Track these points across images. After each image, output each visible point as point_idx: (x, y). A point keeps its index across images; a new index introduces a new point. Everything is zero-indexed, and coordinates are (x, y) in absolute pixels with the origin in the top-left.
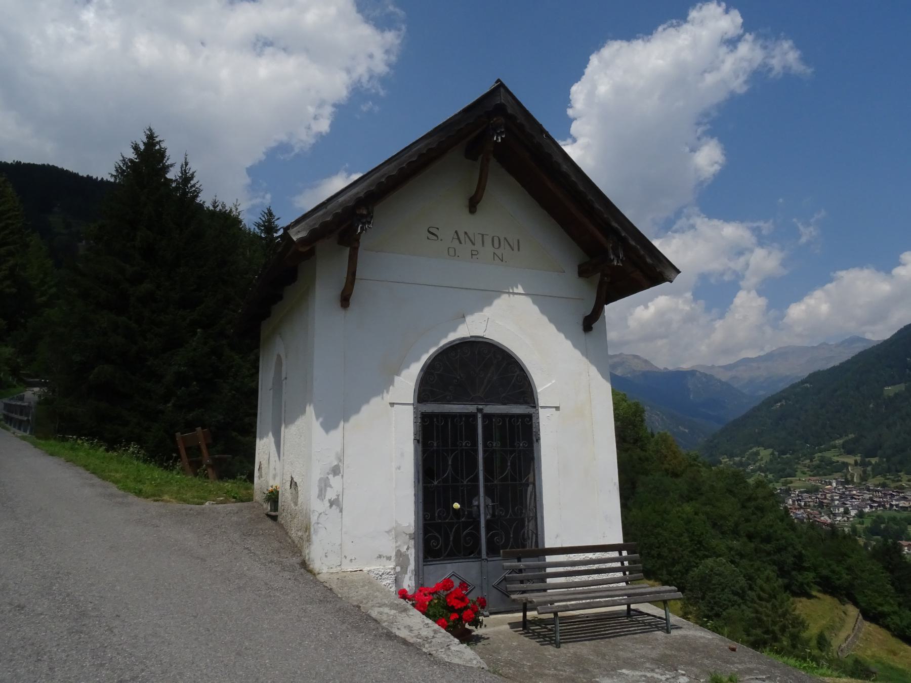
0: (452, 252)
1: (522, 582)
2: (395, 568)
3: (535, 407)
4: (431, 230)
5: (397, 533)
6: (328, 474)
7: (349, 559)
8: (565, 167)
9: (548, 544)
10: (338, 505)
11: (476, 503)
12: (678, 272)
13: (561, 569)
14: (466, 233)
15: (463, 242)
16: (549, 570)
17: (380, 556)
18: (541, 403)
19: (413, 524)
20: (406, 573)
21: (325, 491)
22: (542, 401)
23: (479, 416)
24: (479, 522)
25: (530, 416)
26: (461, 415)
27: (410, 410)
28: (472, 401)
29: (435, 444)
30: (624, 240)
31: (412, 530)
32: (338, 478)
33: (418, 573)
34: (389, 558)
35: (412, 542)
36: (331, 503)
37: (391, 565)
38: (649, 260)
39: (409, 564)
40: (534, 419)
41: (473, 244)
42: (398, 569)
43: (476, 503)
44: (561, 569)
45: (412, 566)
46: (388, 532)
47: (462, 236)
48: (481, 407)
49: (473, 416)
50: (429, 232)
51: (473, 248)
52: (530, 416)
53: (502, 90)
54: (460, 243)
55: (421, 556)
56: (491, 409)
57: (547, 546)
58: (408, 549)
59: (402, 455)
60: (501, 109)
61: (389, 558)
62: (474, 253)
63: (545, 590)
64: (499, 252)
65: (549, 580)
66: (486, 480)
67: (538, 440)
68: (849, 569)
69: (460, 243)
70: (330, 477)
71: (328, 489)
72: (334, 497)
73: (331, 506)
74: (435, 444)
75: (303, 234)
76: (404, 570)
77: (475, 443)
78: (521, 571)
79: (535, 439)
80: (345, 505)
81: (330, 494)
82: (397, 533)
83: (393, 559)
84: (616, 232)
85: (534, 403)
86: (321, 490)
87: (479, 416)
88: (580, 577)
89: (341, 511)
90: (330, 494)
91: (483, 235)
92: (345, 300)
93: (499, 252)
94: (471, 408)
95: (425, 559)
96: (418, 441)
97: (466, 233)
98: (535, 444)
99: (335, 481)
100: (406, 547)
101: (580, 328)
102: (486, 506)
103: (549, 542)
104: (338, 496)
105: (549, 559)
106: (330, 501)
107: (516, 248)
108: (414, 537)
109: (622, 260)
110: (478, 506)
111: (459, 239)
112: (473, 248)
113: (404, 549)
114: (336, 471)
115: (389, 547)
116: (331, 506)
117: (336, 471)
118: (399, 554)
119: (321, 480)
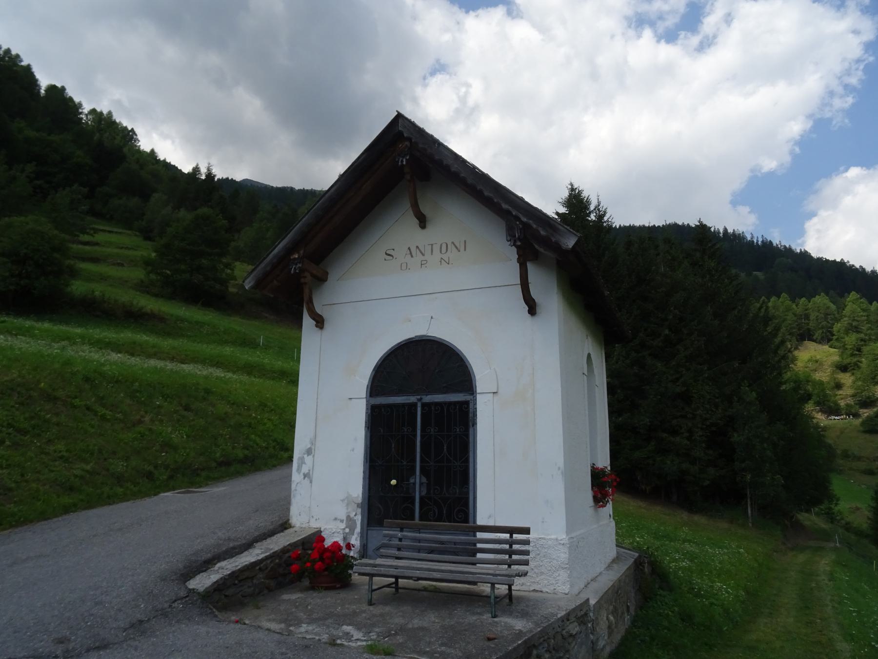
0: (404, 266)
5: (348, 501)
8: (455, 168)
10: (309, 478)
15: (414, 254)
17: (336, 519)
18: (478, 390)
19: (361, 496)
22: (481, 384)
23: (419, 405)
26: (403, 405)
27: (364, 402)
31: (360, 500)
32: (311, 457)
34: (342, 521)
35: (359, 510)
36: (305, 476)
37: (343, 526)
38: (543, 233)
40: (471, 406)
41: (423, 255)
42: (347, 530)
45: (358, 529)
46: (343, 501)
47: (413, 249)
49: (414, 406)
52: (467, 403)
53: (400, 121)
56: (428, 399)
60: (400, 136)
61: (342, 521)
64: (445, 257)
67: (474, 424)
70: (305, 456)
79: (471, 424)
81: (305, 469)
87: (419, 405)
89: (311, 482)
90: (305, 469)
92: (320, 322)
93: (445, 257)
94: (412, 399)
95: (369, 525)
97: (417, 247)
99: (308, 459)
102: (421, 484)
103: (481, 521)
107: (462, 249)
108: (360, 505)
109: (519, 239)
110: (414, 484)
111: (411, 253)
112: (423, 258)
114: (309, 452)
118: (349, 518)
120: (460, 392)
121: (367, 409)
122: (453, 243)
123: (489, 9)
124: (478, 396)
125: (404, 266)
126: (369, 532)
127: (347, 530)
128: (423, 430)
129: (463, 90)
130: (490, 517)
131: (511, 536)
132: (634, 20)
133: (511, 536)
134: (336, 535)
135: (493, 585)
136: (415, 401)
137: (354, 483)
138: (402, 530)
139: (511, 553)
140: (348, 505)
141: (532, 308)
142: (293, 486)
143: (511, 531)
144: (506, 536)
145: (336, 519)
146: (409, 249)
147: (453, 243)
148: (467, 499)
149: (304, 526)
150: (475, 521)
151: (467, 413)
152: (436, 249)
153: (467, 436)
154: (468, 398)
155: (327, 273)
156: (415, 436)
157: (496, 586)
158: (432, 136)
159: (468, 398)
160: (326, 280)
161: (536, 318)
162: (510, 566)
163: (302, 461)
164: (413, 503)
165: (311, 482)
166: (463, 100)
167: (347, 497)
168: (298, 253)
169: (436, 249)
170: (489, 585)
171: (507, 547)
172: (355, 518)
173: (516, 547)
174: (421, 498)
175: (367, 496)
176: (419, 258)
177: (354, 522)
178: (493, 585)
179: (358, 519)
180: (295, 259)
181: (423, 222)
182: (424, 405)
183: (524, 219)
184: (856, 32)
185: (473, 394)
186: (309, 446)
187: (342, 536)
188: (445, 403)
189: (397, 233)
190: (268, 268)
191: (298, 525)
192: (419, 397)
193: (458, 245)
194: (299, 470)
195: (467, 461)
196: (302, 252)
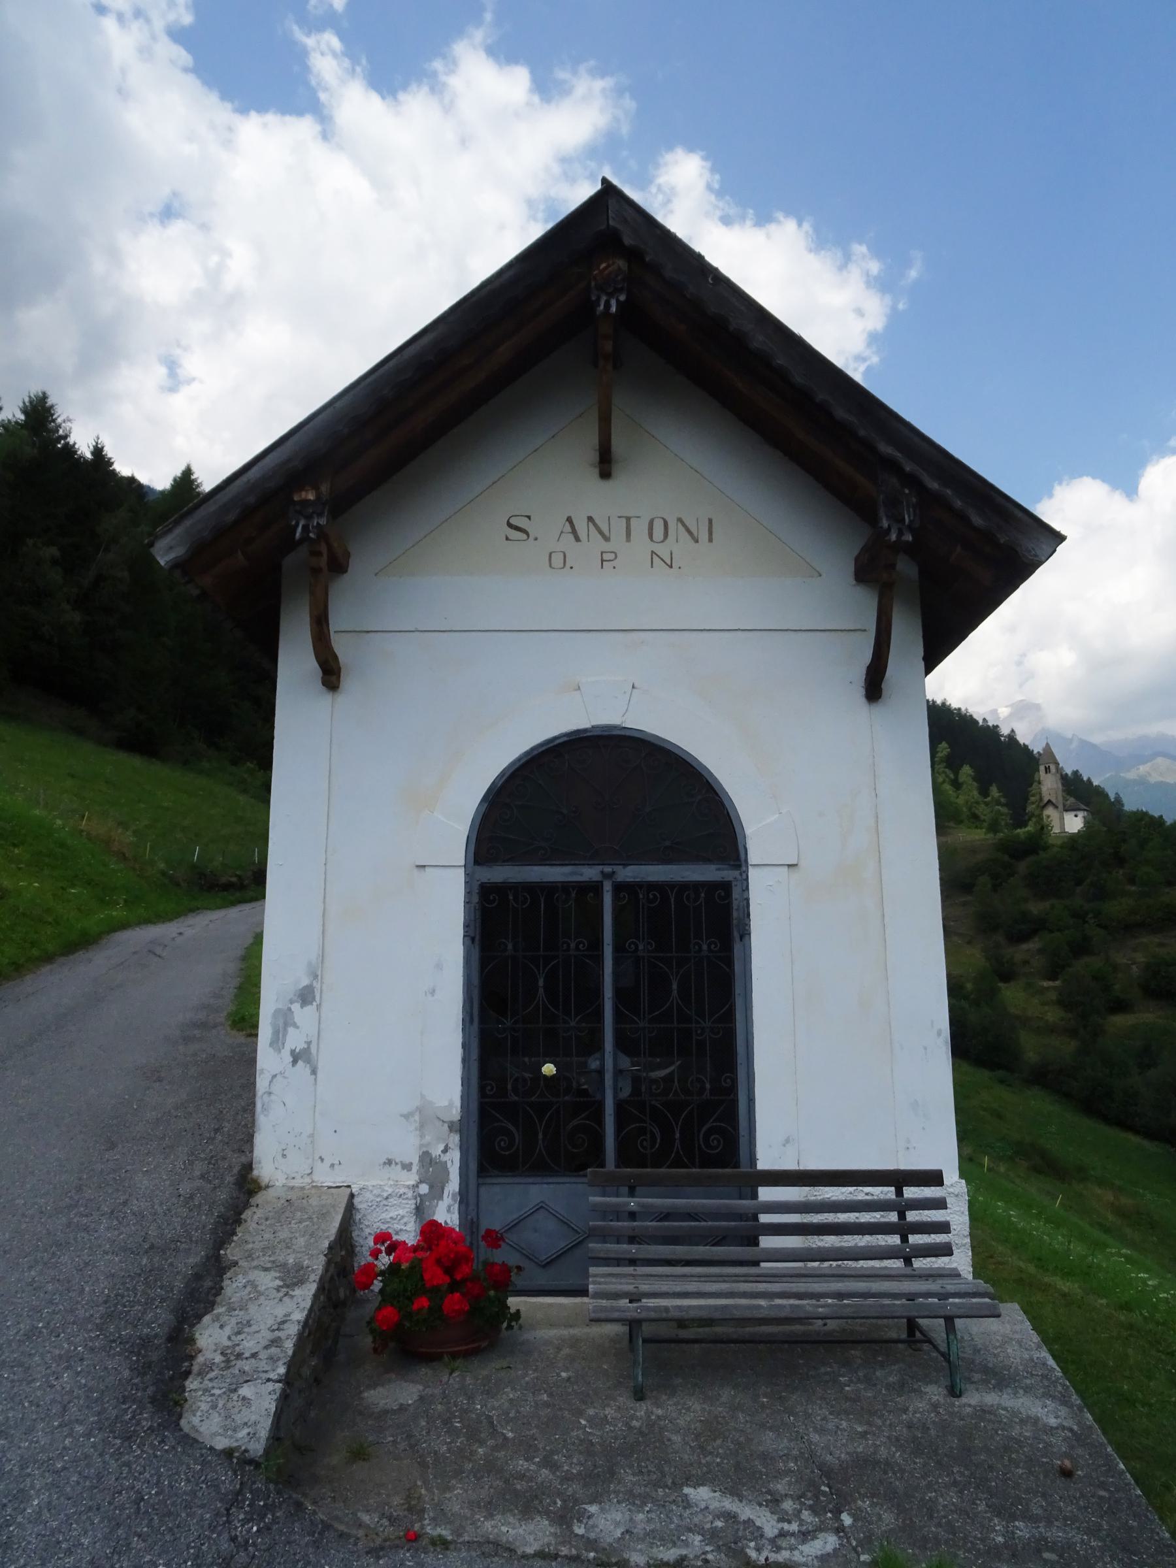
0: (557, 560)
1: (632, 1240)
2: (416, 1186)
3: (738, 867)
4: (513, 521)
5: (423, 1116)
6: (292, 1002)
7: (327, 1162)
8: (758, 340)
9: (764, 1162)
10: (308, 1061)
11: (594, 1064)
12: (1060, 538)
13: (843, 1217)
14: (590, 519)
15: (582, 534)
16: (764, 1218)
17: (389, 1162)
18: (753, 858)
19: (458, 1103)
20: (441, 1197)
21: (285, 1035)
22: (756, 851)
23: (608, 886)
24: (601, 1105)
25: (726, 887)
26: (566, 887)
27: (460, 875)
28: (593, 858)
29: (510, 947)
30: (912, 481)
31: (455, 1114)
32: (310, 1009)
33: (464, 1197)
34: (407, 1167)
35: (455, 1139)
36: (296, 1057)
37: (411, 1178)
38: (977, 520)
39: (446, 1179)
40: (736, 893)
41: (607, 539)
42: (424, 1189)
43: (594, 1064)
44: (843, 1217)
45: (453, 1185)
46: (406, 1116)
47: (581, 526)
48: (608, 869)
49: (595, 888)
50: (510, 525)
51: (606, 546)
52: (726, 887)
53: (612, 203)
54: (577, 539)
55: (473, 1166)
56: (629, 873)
57: (763, 1164)
58: (445, 1151)
59: (439, 966)
60: (610, 242)
61: (407, 1167)
62: (606, 557)
63: (756, 1263)
64: (663, 550)
65: (768, 1242)
66: (618, 1015)
67: (745, 934)
68: (827, 1382)
69: (577, 539)
70: (296, 1007)
71: (291, 1030)
72: (300, 1046)
73: (295, 1062)
74: (510, 947)
75: (179, 552)
76: (437, 1191)
77: (596, 945)
78: (632, 1216)
79: (736, 934)
80: (324, 1061)
81: (295, 1040)
82: (423, 1116)
83: (415, 1168)
84: (892, 466)
85: (738, 858)
86: (276, 1033)
87: (608, 886)
88: (867, 1238)
89: (314, 1072)
90: (295, 1040)
91: (628, 519)
92: (331, 674)
93: (663, 550)
94: (589, 873)
95: (482, 1171)
96: (473, 939)
97: (590, 519)
98: (737, 947)
99: (303, 1015)
100: (441, 1147)
101: (859, 691)
102: (618, 1072)
103: (770, 1154)
104: (309, 1043)
105: (767, 1194)
106: (293, 1052)
107: (704, 536)
108: (460, 1127)
109: (910, 528)
110: (601, 1072)
111: (574, 532)
112: (606, 546)
113: (437, 1151)
114: (306, 996)
115: (408, 1147)
116: (295, 1062)
117: (306, 996)
118: (426, 1159)
119: (277, 1012)
120: (707, 860)
121: (468, 893)
122: (680, 520)
123: (288, 118)
124: (752, 873)
125: (557, 560)
126: (483, 1189)
127: (424, 1189)
128: (618, 949)
129: (215, 259)
130: (787, 1141)
131: (899, 1193)
132: (542, 207)
133: (899, 1193)
134: (392, 1201)
135: (949, 1320)
136: (598, 878)
137: (436, 1070)
138: (632, 1193)
139: (904, 1229)
140: (422, 1126)
141: (874, 688)
142: (262, 1084)
143: (899, 1179)
144: (888, 1193)
145: (389, 1162)
146: (569, 520)
147: (680, 520)
148: (734, 1103)
149: (297, 1183)
150: (753, 1160)
151: (728, 908)
152: (639, 528)
153: (730, 962)
154: (728, 874)
155: (348, 555)
156: (599, 959)
157: (959, 1323)
158: (699, 258)
159: (728, 874)
160: (346, 571)
161: (878, 709)
162: (908, 1262)
163: (285, 1020)
164: (599, 1118)
165: (314, 1072)
166: (214, 276)
167: (420, 1110)
168: (316, 488)
169: (639, 528)
170: (942, 1321)
171: (893, 1217)
172: (444, 1158)
173: (912, 1216)
174: (620, 1106)
175: (474, 1106)
176: (598, 544)
177: (444, 1169)
178: (949, 1320)
179: (454, 1160)
180: (305, 502)
181: (606, 465)
182: (620, 888)
183: (934, 485)
184: (860, 312)
185: (738, 867)
186: (305, 982)
187: (411, 1205)
188: (672, 885)
189: (539, 481)
190: (231, 517)
191: (280, 1180)
192: (608, 869)
193: (694, 529)
194: (277, 1041)
195: (729, 1017)
196: (324, 488)
